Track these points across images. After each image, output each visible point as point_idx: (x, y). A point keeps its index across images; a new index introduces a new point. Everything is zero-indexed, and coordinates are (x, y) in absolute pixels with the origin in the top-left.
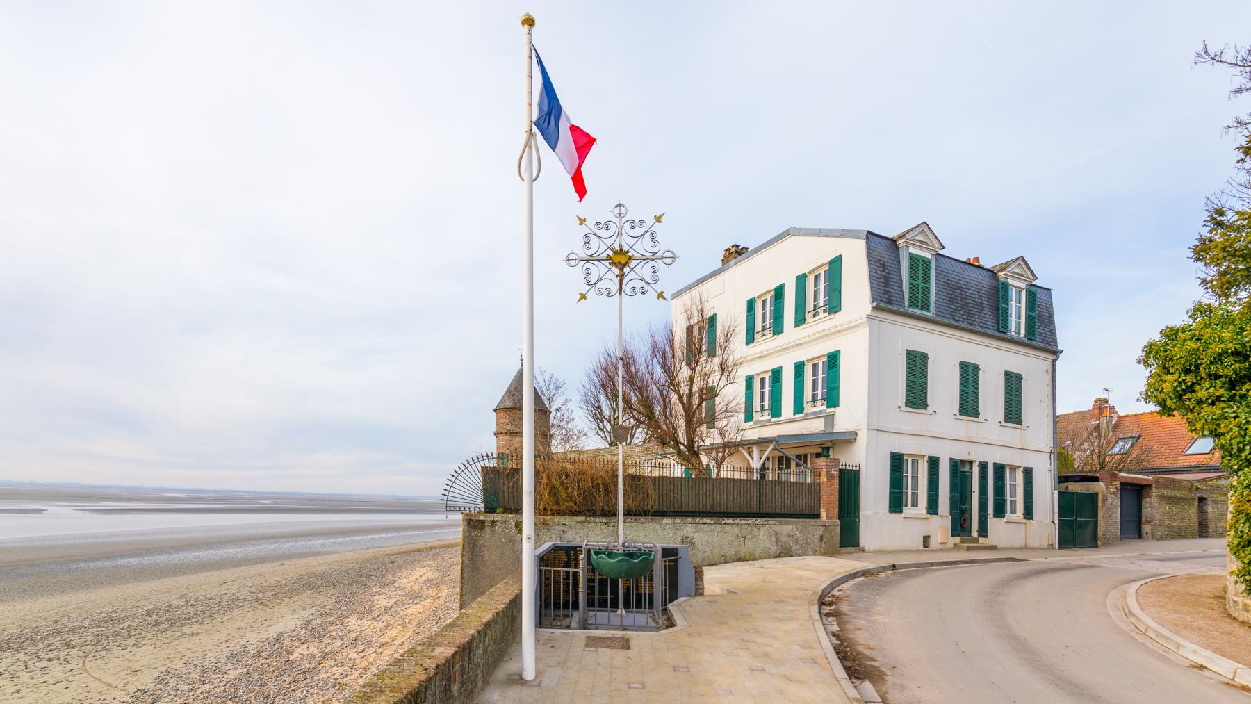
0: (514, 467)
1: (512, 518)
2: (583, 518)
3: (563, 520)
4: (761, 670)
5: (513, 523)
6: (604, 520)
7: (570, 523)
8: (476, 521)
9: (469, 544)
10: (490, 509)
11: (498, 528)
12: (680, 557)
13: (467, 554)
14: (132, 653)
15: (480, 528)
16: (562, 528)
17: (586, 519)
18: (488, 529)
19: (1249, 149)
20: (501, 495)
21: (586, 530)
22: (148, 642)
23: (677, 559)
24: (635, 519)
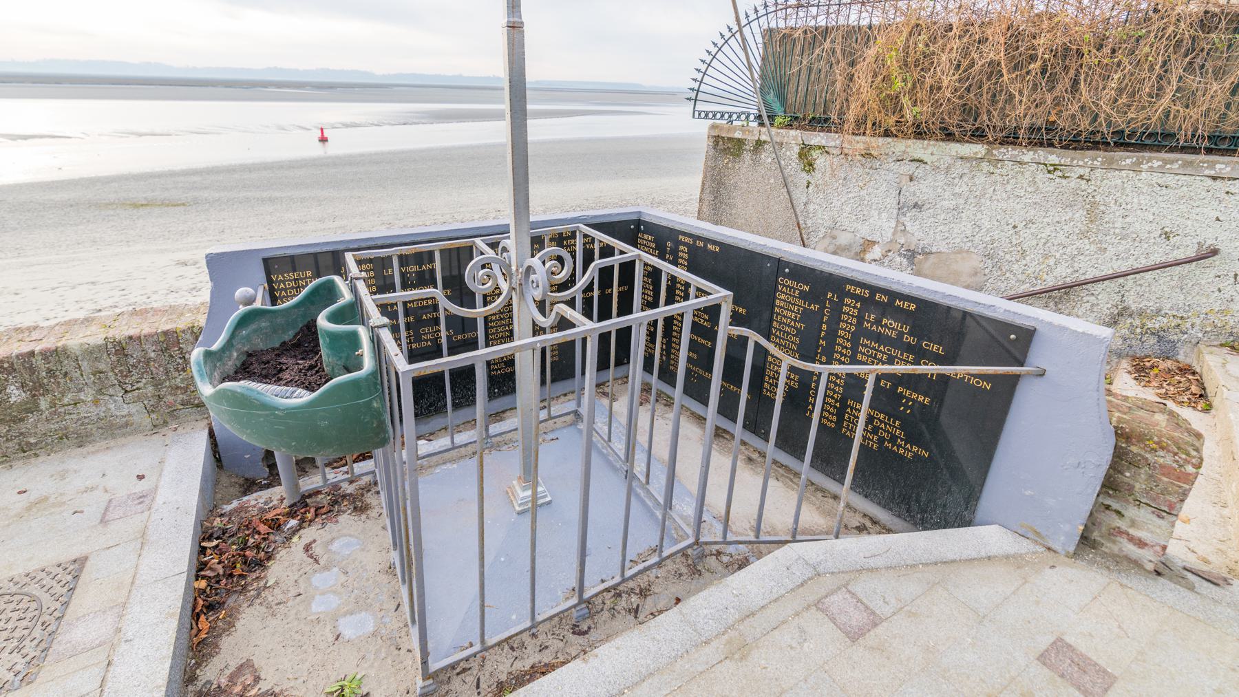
0: (822, 21)
1: (795, 138)
2: (979, 149)
3: (917, 148)
4: (104, 515)
5: (797, 149)
6: (1053, 158)
7: (935, 158)
8: (730, 139)
9: (713, 181)
10: (766, 118)
11: (766, 157)
12: (1042, 374)
13: (708, 198)
14: (62, 584)
15: (732, 154)
16: (909, 168)
17: (989, 152)
18: (747, 157)
19: (3, 419)
20: (792, 88)
21: (981, 179)
22: (18, 623)
23: (1016, 378)
24: (1187, 164)
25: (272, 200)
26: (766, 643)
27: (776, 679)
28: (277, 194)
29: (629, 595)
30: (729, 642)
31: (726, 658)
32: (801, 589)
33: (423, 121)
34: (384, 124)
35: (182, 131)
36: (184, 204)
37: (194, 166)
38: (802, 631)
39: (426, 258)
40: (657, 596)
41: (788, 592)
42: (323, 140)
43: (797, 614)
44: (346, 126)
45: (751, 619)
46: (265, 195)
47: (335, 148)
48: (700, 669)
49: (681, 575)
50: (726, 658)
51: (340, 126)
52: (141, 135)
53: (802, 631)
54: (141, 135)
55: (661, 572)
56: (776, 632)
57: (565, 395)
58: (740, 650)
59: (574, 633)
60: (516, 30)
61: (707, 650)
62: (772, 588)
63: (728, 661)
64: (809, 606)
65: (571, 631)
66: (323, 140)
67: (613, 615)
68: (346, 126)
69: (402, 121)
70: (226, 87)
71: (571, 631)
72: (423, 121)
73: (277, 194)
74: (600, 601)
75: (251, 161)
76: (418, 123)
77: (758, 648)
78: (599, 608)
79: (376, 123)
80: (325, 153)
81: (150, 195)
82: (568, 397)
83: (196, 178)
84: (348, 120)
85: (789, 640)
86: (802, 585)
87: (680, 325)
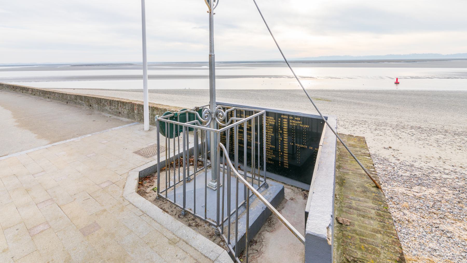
25: (359, 104)
26: (177, 249)
27: (164, 253)
28: (363, 102)
29: (195, 222)
30: (175, 239)
31: (169, 239)
32: (204, 257)
33: (462, 77)
34: (435, 77)
35: (344, 77)
36: (330, 101)
37: (341, 89)
38: (184, 258)
39: (251, 113)
40: (197, 229)
41: (200, 252)
42: (397, 83)
43: (191, 256)
44: (412, 78)
45: (185, 244)
46: (358, 102)
47: (401, 87)
48: (164, 234)
49: (208, 232)
50: (169, 239)
51: (410, 78)
52: (332, 78)
53: (184, 258)
54: (332, 78)
55: (206, 227)
56: (182, 251)
57: (292, 186)
58: (173, 242)
59: (178, 215)
60: (210, 56)
61: (171, 235)
62: (200, 247)
63: (168, 240)
64: (196, 260)
65: (179, 214)
66: (397, 83)
67: (187, 221)
68: (412, 78)
69: (448, 77)
70: (368, 62)
71: (179, 214)
72: (462, 77)
73: (363, 102)
74: (190, 216)
75: (345, 89)
76: (458, 78)
77: (175, 247)
78: (188, 217)
79: (430, 77)
80: (397, 88)
81: (323, 96)
82: (292, 188)
83: (339, 93)
84: (414, 75)
85: (179, 255)
86: (206, 257)
87: (268, 152)
